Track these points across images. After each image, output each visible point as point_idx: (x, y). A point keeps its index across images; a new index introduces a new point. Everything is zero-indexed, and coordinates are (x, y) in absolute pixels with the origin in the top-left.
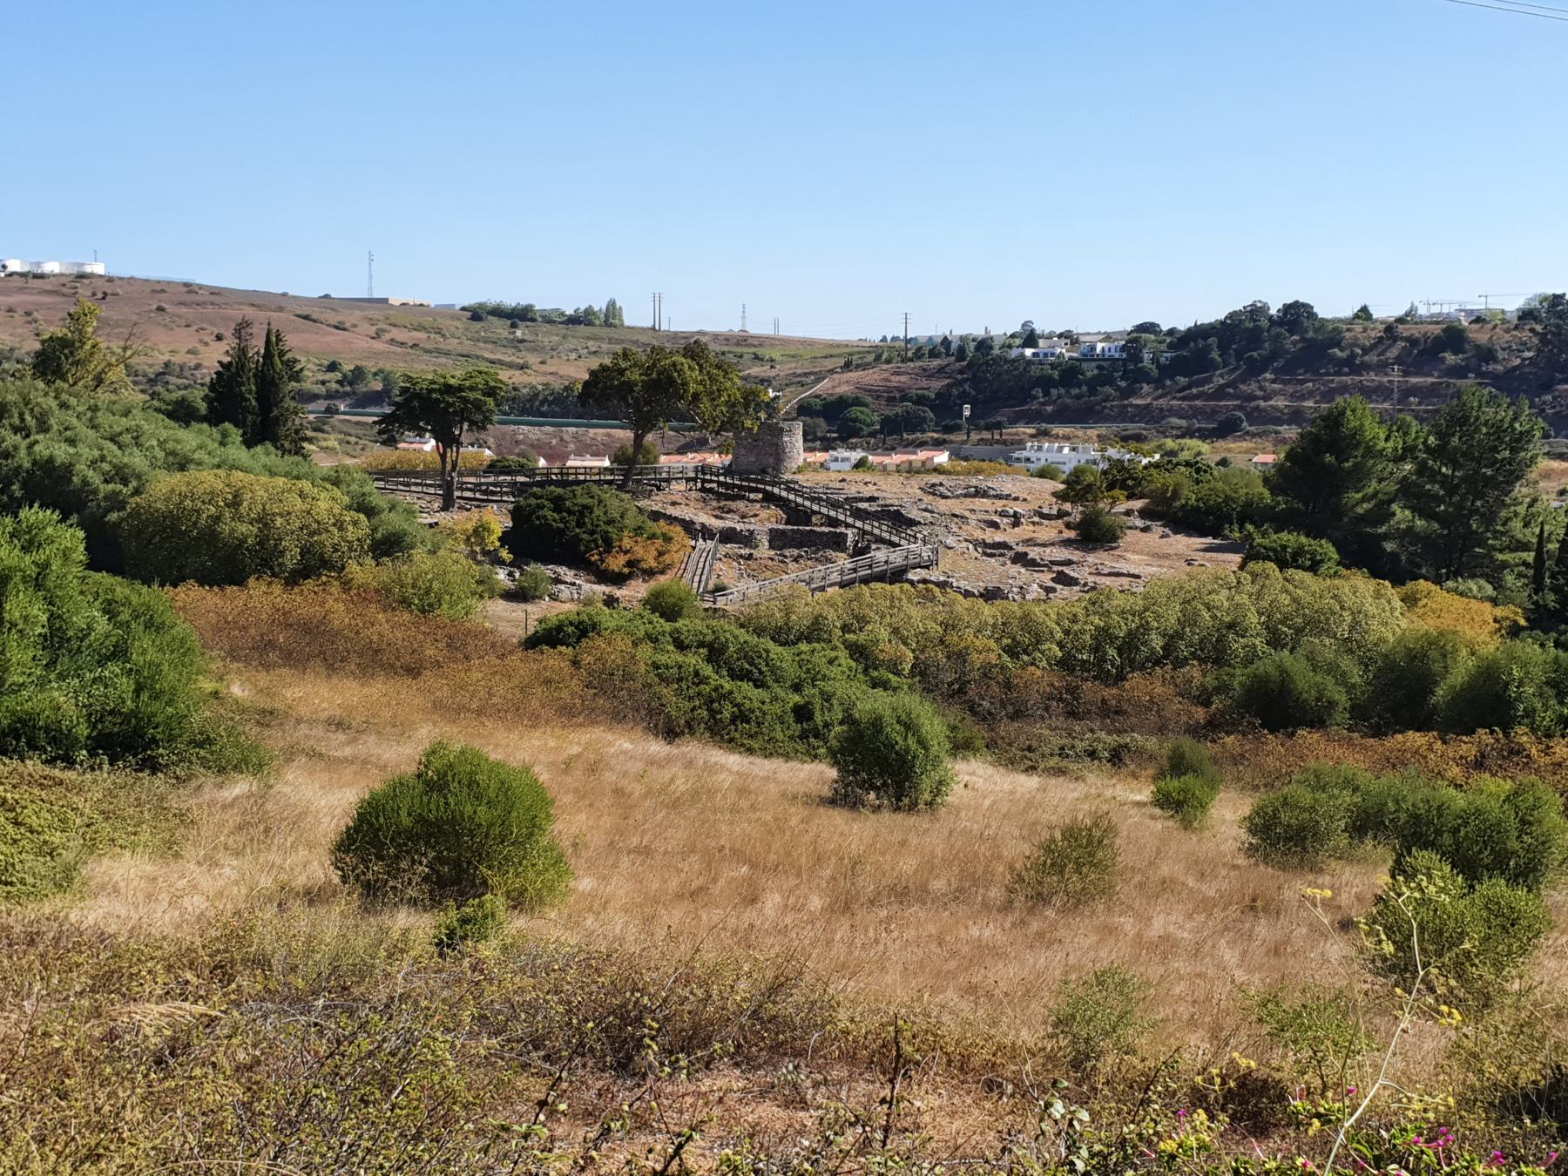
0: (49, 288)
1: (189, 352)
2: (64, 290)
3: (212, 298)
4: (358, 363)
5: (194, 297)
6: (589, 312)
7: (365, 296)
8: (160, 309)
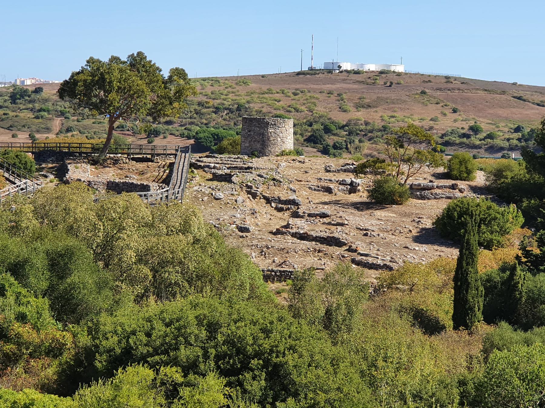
0: (360, 79)
1: (431, 120)
2: (369, 81)
3: (463, 86)
4: (520, 124)
5: (450, 86)
6: (516, 83)
7: (298, 70)
8: (423, 93)
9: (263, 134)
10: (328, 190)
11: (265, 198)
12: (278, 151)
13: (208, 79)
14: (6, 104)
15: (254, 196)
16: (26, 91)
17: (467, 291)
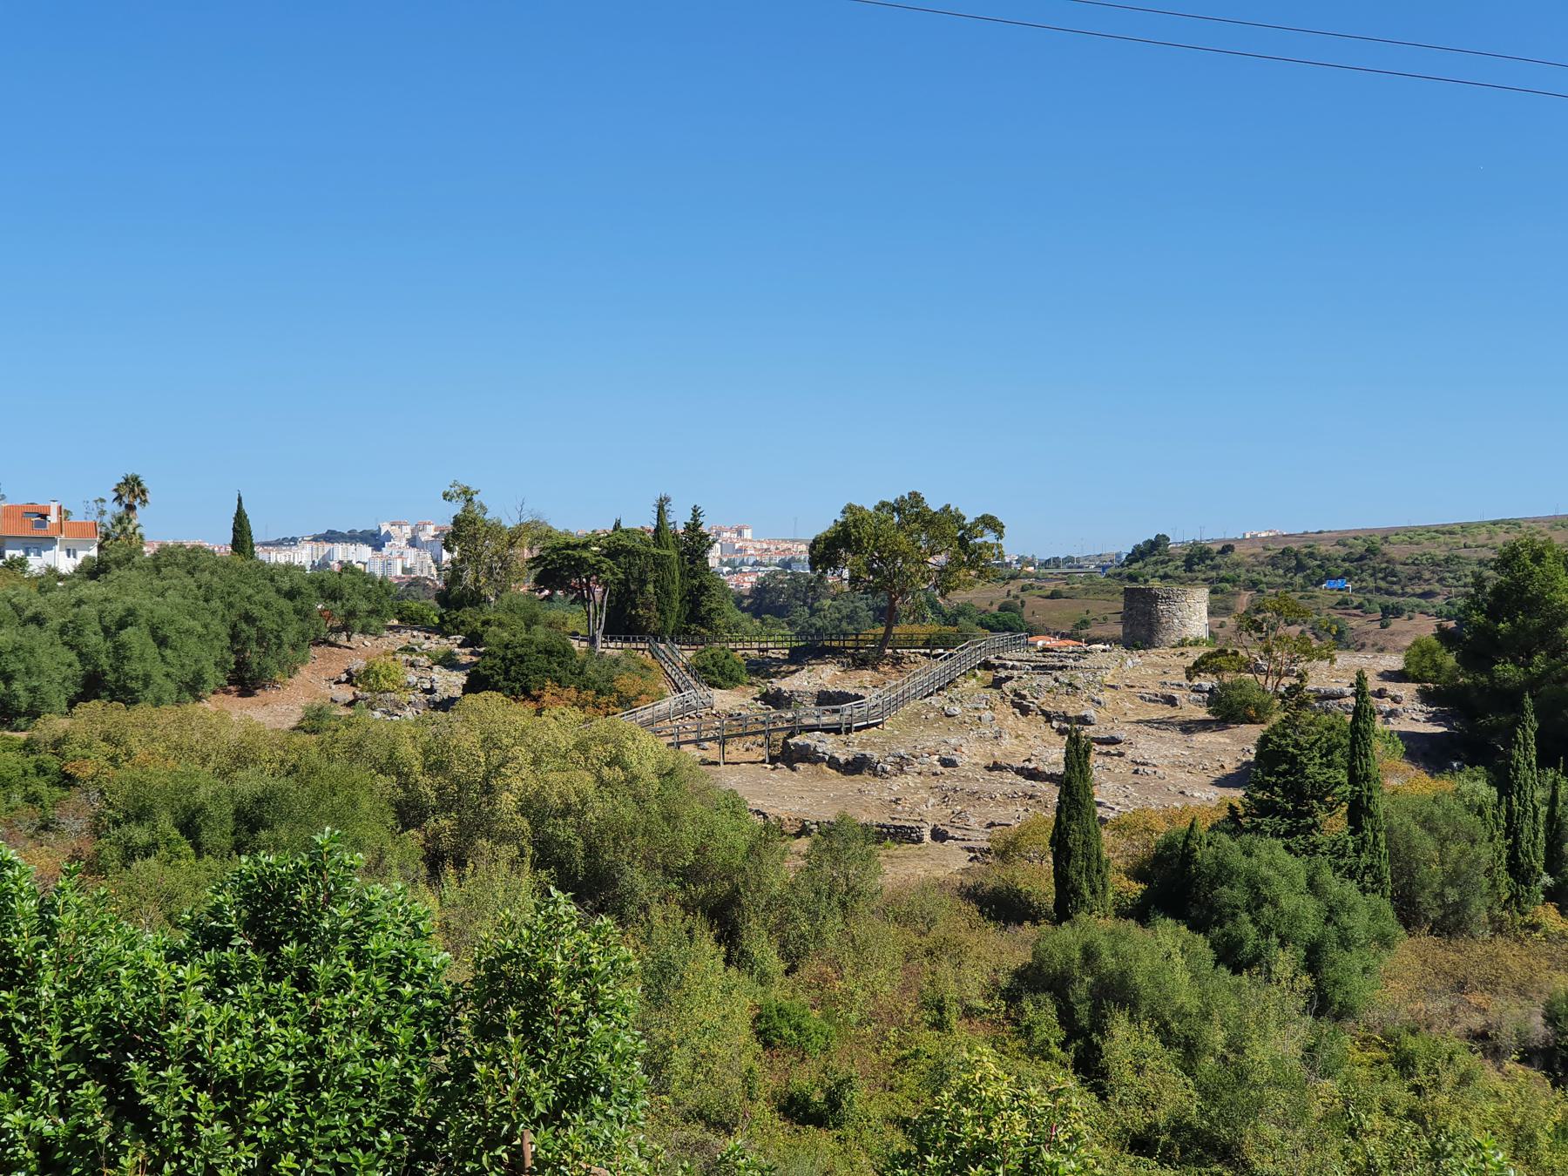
9: (1150, 613)
10: (1171, 701)
11: (1044, 713)
12: (1176, 640)
13: (1502, 521)
14: (1178, 573)
15: (1025, 711)
16: (1208, 552)
17: (1068, 863)
